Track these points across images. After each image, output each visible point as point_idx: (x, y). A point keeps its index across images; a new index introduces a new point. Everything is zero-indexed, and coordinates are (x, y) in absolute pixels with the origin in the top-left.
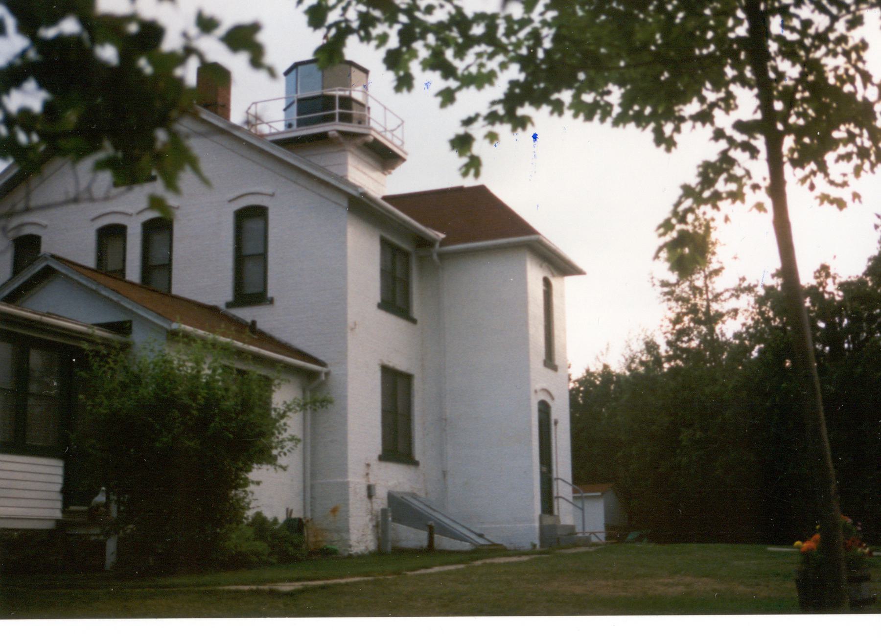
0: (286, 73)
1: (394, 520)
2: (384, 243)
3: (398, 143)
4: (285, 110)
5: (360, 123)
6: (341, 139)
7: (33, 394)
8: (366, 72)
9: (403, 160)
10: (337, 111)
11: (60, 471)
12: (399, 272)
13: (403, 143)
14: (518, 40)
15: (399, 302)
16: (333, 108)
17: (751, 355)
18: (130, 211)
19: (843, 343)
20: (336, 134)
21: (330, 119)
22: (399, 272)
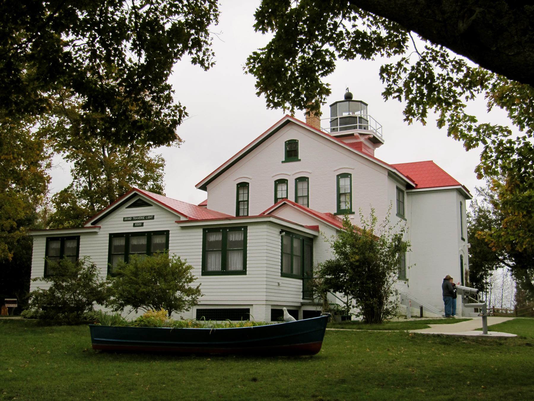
0: (331, 106)
1: (198, 310)
2: (397, 188)
3: (380, 136)
4: (330, 122)
5: (365, 129)
6: (359, 136)
7: (295, 255)
8: (366, 105)
9: (383, 144)
10: (358, 124)
11: (302, 284)
12: (401, 200)
13: (382, 136)
14: (345, 33)
15: (401, 213)
16: (357, 123)
17: (108, 108)
18: (289, 174)
19: (30, 16)
20: (358, 135)
21: (355, 127)
22: (401, 200)
